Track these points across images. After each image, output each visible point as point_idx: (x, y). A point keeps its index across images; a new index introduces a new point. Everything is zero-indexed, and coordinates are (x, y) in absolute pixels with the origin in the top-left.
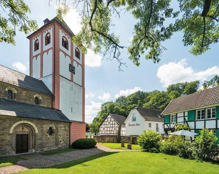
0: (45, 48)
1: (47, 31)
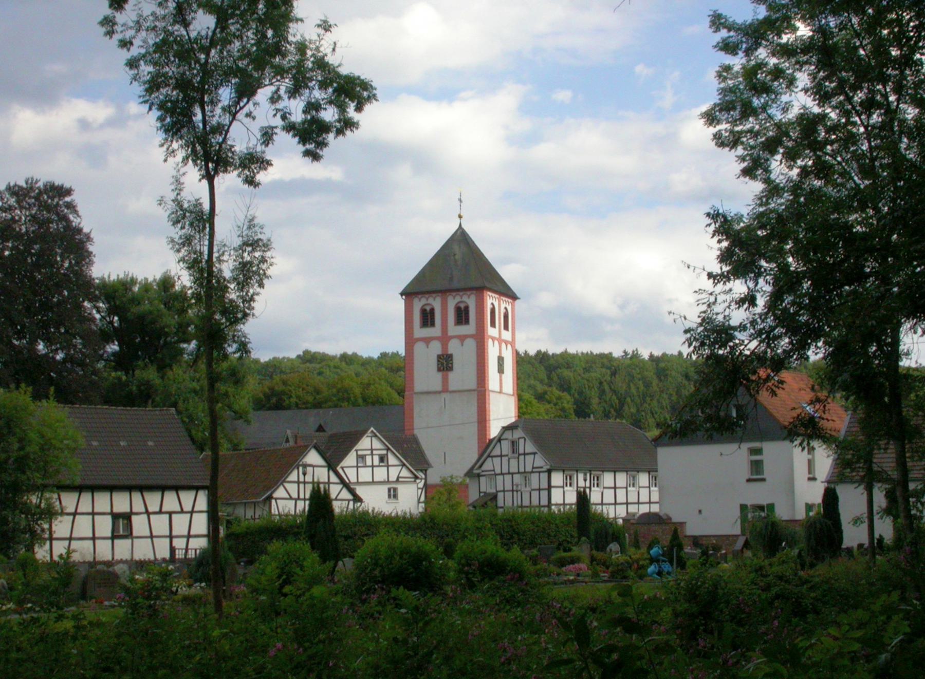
0: (454, 330)
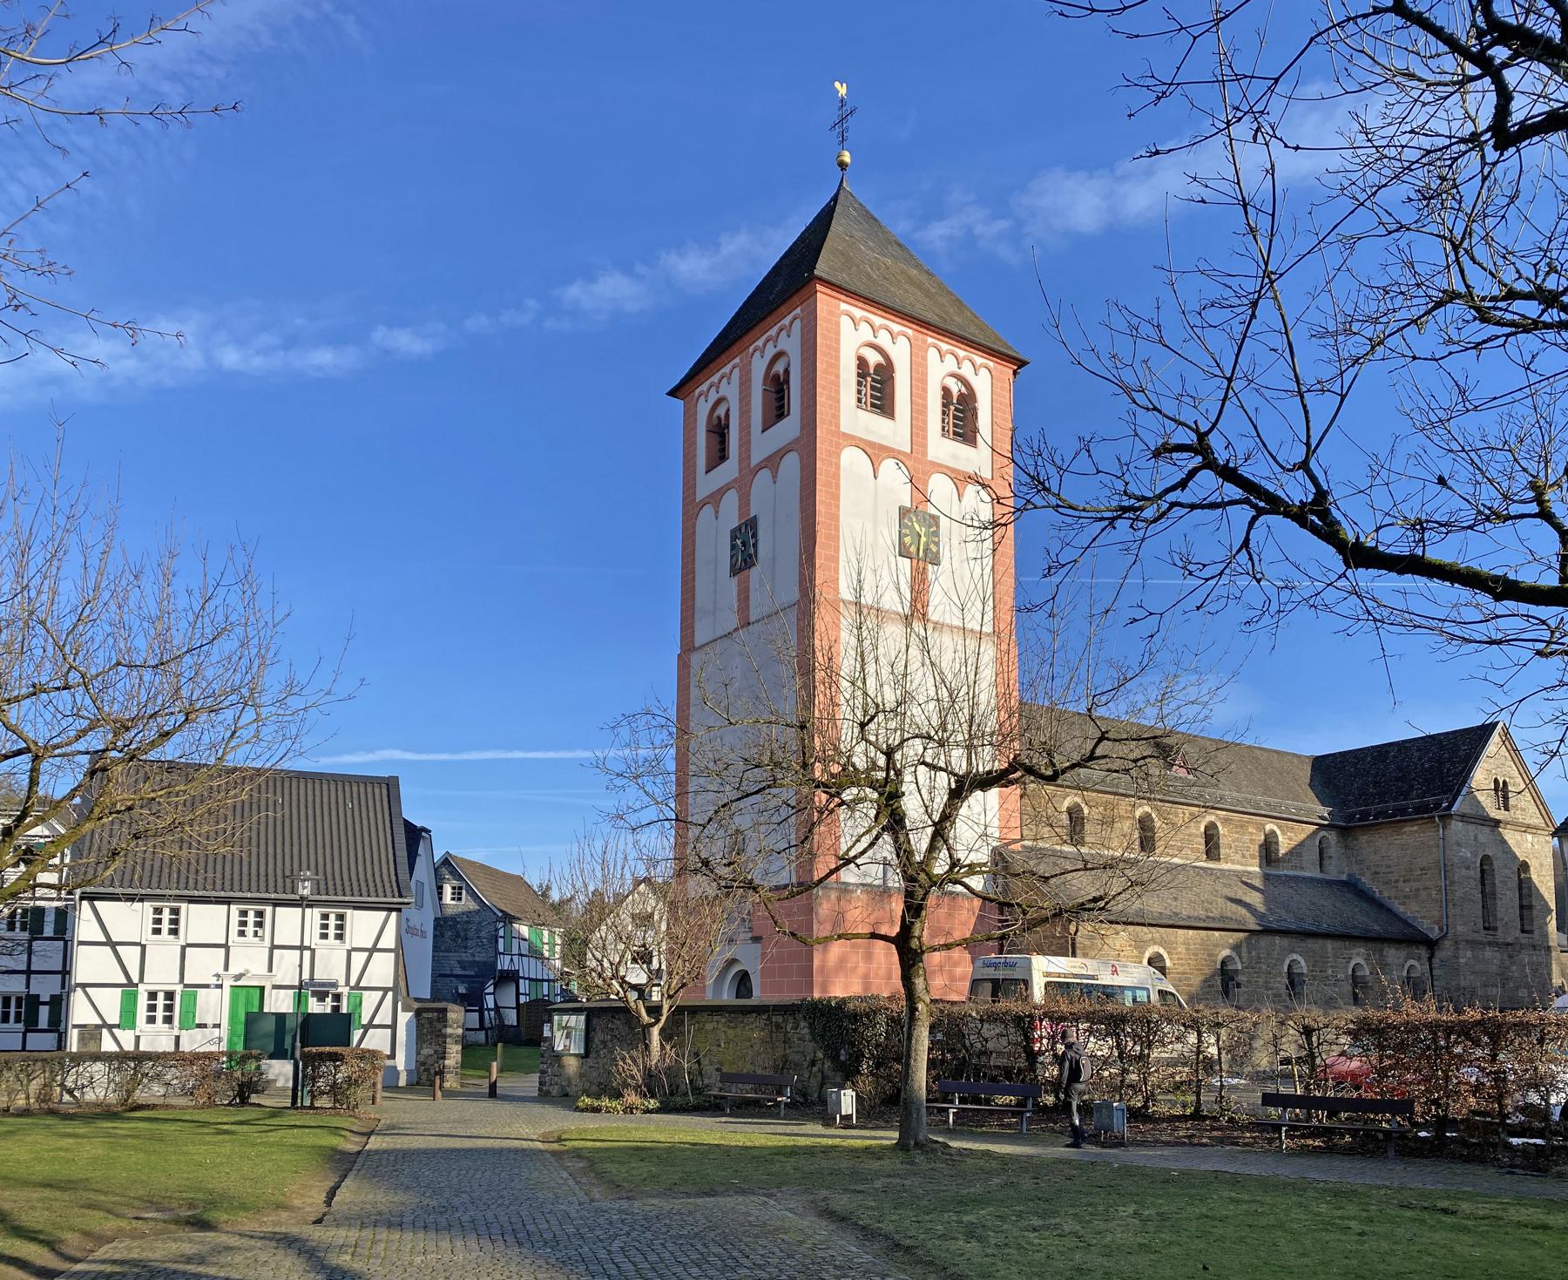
0: (764, 444)
1: (771, 343)
